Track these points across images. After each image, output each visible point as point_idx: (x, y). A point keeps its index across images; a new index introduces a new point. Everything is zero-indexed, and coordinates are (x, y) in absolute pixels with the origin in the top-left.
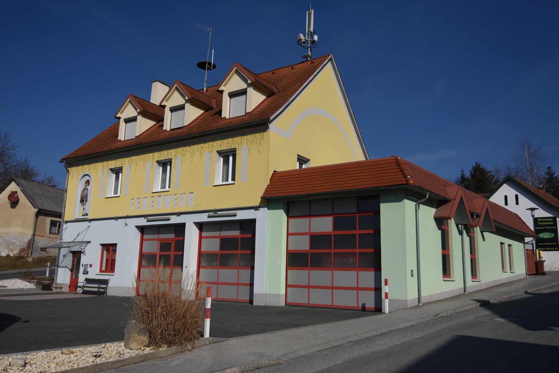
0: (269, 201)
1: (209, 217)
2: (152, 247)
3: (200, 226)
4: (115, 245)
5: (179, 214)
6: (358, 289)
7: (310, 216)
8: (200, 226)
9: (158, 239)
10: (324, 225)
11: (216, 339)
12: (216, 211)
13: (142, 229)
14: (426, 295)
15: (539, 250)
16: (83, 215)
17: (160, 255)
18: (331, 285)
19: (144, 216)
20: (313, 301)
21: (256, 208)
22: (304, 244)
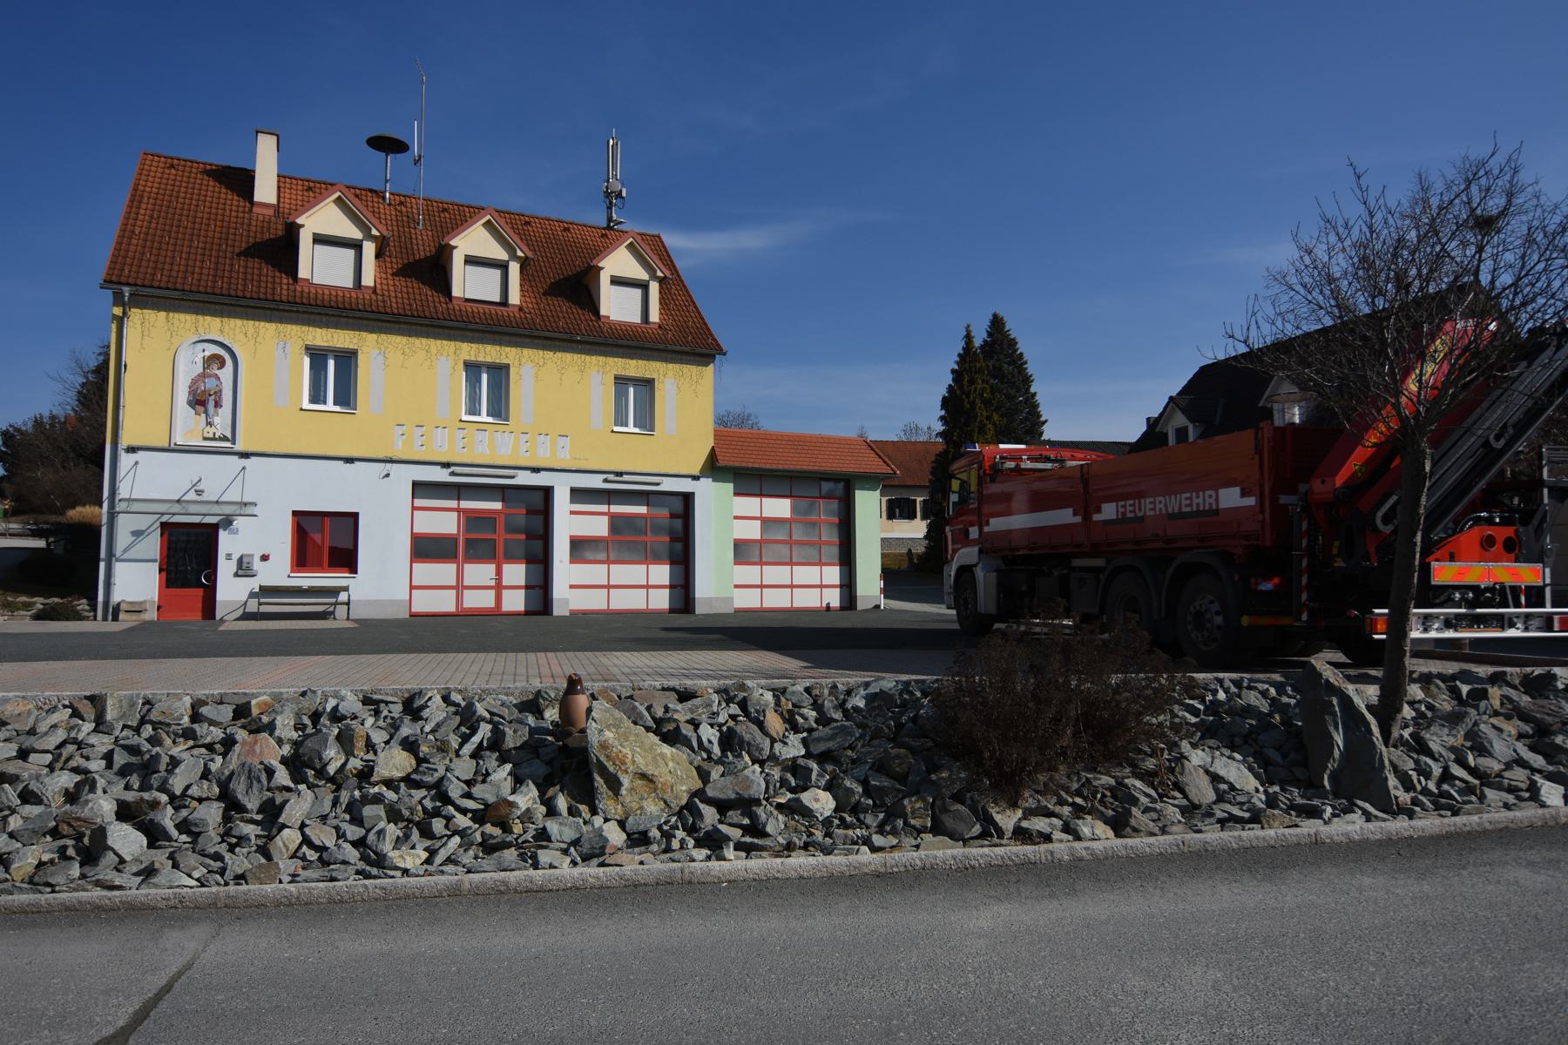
0: (714, 468)
1: (606, 481)
2: (443, 521)
3: (578, 494)
4: (355, 516)
5: (536, 470)
6: (821, 586)
7: (761, 495)
8: (578, 494)
9: (458, 510)
10: (780, 507)
11: (1535, 522)
12: (620, 474)
13: (419, 488)
14: (712, 594)
15: (504, 302)
16: (205, 439)
17: (468, 541)
18: (505, 583)
19: (446, 465)
20: (614, 606)
21: (696, 478)
22: (753, 531)
